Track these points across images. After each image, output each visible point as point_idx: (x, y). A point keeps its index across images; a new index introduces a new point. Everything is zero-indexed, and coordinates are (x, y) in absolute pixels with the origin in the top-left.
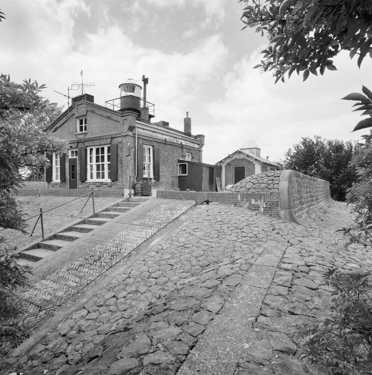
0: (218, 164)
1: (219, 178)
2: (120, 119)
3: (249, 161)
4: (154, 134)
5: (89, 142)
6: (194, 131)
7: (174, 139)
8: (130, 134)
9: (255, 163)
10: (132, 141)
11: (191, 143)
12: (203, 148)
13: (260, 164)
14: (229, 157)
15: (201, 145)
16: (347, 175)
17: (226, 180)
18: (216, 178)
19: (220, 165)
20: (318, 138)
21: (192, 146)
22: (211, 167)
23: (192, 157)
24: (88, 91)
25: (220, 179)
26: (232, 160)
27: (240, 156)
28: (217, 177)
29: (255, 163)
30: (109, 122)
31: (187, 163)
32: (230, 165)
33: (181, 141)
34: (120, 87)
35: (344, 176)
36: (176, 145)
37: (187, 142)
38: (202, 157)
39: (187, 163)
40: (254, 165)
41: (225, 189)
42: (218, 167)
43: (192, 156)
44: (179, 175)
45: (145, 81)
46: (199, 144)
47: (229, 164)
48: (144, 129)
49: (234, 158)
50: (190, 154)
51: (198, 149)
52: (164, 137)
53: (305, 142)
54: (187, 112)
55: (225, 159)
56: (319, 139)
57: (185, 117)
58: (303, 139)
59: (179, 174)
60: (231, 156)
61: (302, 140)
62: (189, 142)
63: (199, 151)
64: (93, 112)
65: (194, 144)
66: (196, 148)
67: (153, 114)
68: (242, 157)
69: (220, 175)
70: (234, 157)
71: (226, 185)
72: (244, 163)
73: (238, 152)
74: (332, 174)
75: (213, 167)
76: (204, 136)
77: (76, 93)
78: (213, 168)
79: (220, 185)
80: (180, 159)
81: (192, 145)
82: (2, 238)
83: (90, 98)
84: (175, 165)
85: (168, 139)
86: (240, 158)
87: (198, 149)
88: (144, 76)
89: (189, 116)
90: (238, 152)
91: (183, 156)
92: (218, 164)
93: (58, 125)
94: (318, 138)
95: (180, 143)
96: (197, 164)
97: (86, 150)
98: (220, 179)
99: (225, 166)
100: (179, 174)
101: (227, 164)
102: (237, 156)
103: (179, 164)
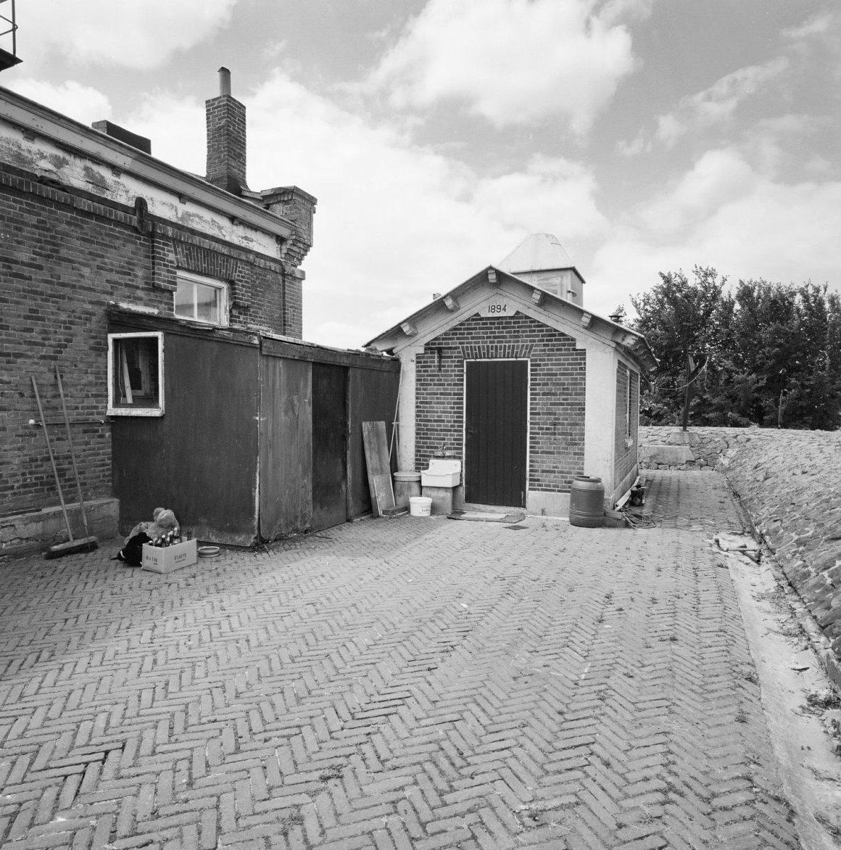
0: (381, 348)
1: (382, 425)
3: (553, 334)
6: (259, 179)
7: (60, 163)
9: (584, 341)
11: (225, 222)
12: (307, 265)
13: (619, 348)
14: (438, 306)
15: (297, 244)
16: (810, 394)
17: (422, 433)
18: (366, 426)
19: (390, 352)
20: (706, 274)
21: (236, 241)
22: (330, 360)
23: (235, 306)
25: (389, 428)
26: (455, 323)
27: (501, 301)
28: (373, 418)
29: (584, 341)
31: (159, 335)
32: (446, 353)
35: (799, 399)
36: (85, 204)
37: (190, 208)
38: (298, 309)
39: (159, 335)
40: (583, 352)
41: (415, 488)
42: (380, 360)
43: (233, 295)
44: (112, 411)
46: (280, 240)
47: (436, 348)
49: (466, 316)
50: (224, 286)
51: (273, 266)
54: (225, 72)
55: (415, 319)
56: (710, 280)
57: (216, 92)
58: (664, 277)
59: (117, 404)
60: (449, 303)
61: (661, 282)
62: (208, 215)
63: (284, 274)
65: (250, 234)
66: (258, 255)
68: (511, 305)
69: (387, 409)
70: (469, 308)
71: (421, 464)
72: (524, 341)
73: (492, 278)
74: (759, 390)
75: (345, 362)
76: (312, 201)
78: (346, 369)
79: (387, 459)
80: (124, 305)
81: (235, 235)
84: (81, 342)
86: (502, 314)
87: (273, 266)
90: (492, 278)
91: (155, 288)
92: (381, 348)
94: (706, 274)
95: (132, 204)
96: (224, 342)
98: (389, 428)
99: (418, 356)
100: (117, 404)
101: (428, 347)
102: (481, 305)
103: (111, 337)
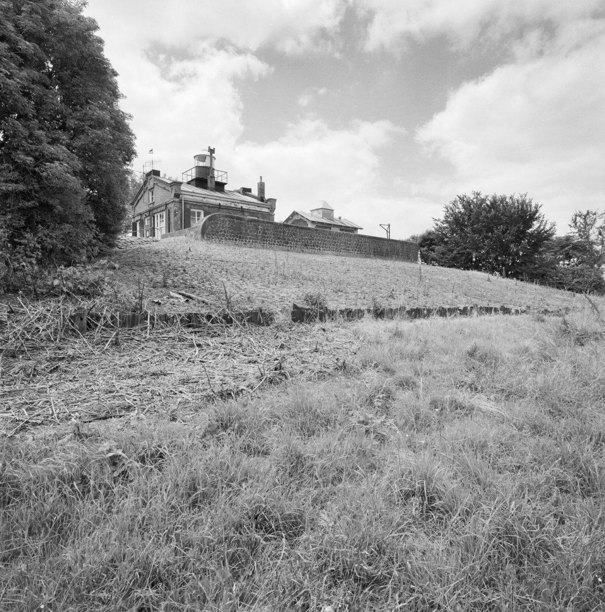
2: (170, 189)
4: (205, 200)
5: (170, 216)
8: (177, 200)
10: (179, 206)
15: (272, 209)
24: (156, 169)
30: (165, 192)
33: (241, 205)
34: (194, 157)
45: (212, 151)
48: (192, 196)
52: (218, 202)
53: (467, 204)
54: (261, 177)
64: (157, 184)
67: (226, 182)
77: (148, 170)
82: (4, 35)
83: (157, 173)
85: (222, 203)
88: (209, 147)
89: (263, 181)
93: (139, 198)
97: (154, 217)
